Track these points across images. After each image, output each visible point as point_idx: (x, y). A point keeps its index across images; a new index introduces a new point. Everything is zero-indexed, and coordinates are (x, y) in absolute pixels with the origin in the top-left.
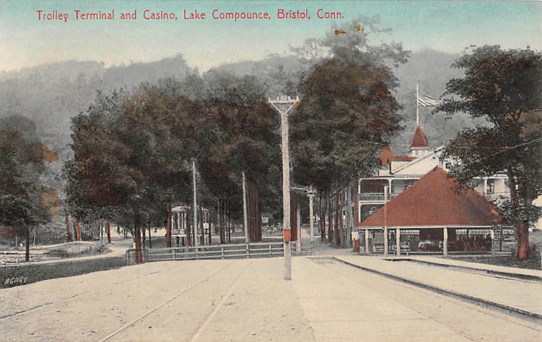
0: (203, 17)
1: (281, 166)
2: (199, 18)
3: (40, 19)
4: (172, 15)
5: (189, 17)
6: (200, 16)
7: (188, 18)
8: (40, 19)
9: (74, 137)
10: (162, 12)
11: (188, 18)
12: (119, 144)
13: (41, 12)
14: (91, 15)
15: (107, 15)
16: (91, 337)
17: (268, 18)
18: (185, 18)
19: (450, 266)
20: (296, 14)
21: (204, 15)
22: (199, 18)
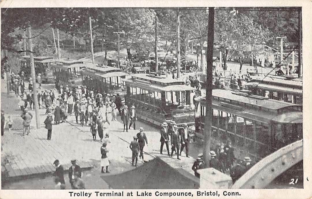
0: (150, 195)
1: (58, 9)
2: (147, 195)
3: (97, 196)
4: (225, 192)
5: (141, 194)
6: (148, 194)
7: (140, 195)
8: (97, 196)
9: (71, 78)
10: (205, 191)
11: (140, 195)
12: (82, 55)
13: (72, 193)
14: (107, 194)
15: (118, 194)
16: (241, 72)
17: (191, 196)
18: (137, 195)
19: (2, 148)
20: (210, 194)
21: (151, 194)
22: (147, 195)
